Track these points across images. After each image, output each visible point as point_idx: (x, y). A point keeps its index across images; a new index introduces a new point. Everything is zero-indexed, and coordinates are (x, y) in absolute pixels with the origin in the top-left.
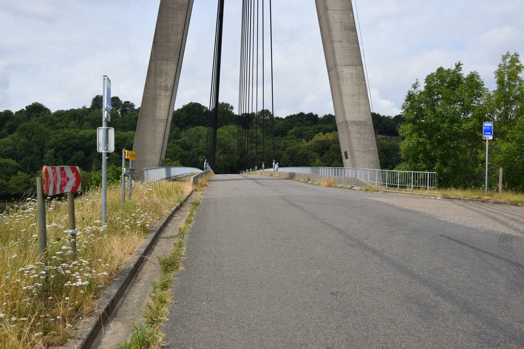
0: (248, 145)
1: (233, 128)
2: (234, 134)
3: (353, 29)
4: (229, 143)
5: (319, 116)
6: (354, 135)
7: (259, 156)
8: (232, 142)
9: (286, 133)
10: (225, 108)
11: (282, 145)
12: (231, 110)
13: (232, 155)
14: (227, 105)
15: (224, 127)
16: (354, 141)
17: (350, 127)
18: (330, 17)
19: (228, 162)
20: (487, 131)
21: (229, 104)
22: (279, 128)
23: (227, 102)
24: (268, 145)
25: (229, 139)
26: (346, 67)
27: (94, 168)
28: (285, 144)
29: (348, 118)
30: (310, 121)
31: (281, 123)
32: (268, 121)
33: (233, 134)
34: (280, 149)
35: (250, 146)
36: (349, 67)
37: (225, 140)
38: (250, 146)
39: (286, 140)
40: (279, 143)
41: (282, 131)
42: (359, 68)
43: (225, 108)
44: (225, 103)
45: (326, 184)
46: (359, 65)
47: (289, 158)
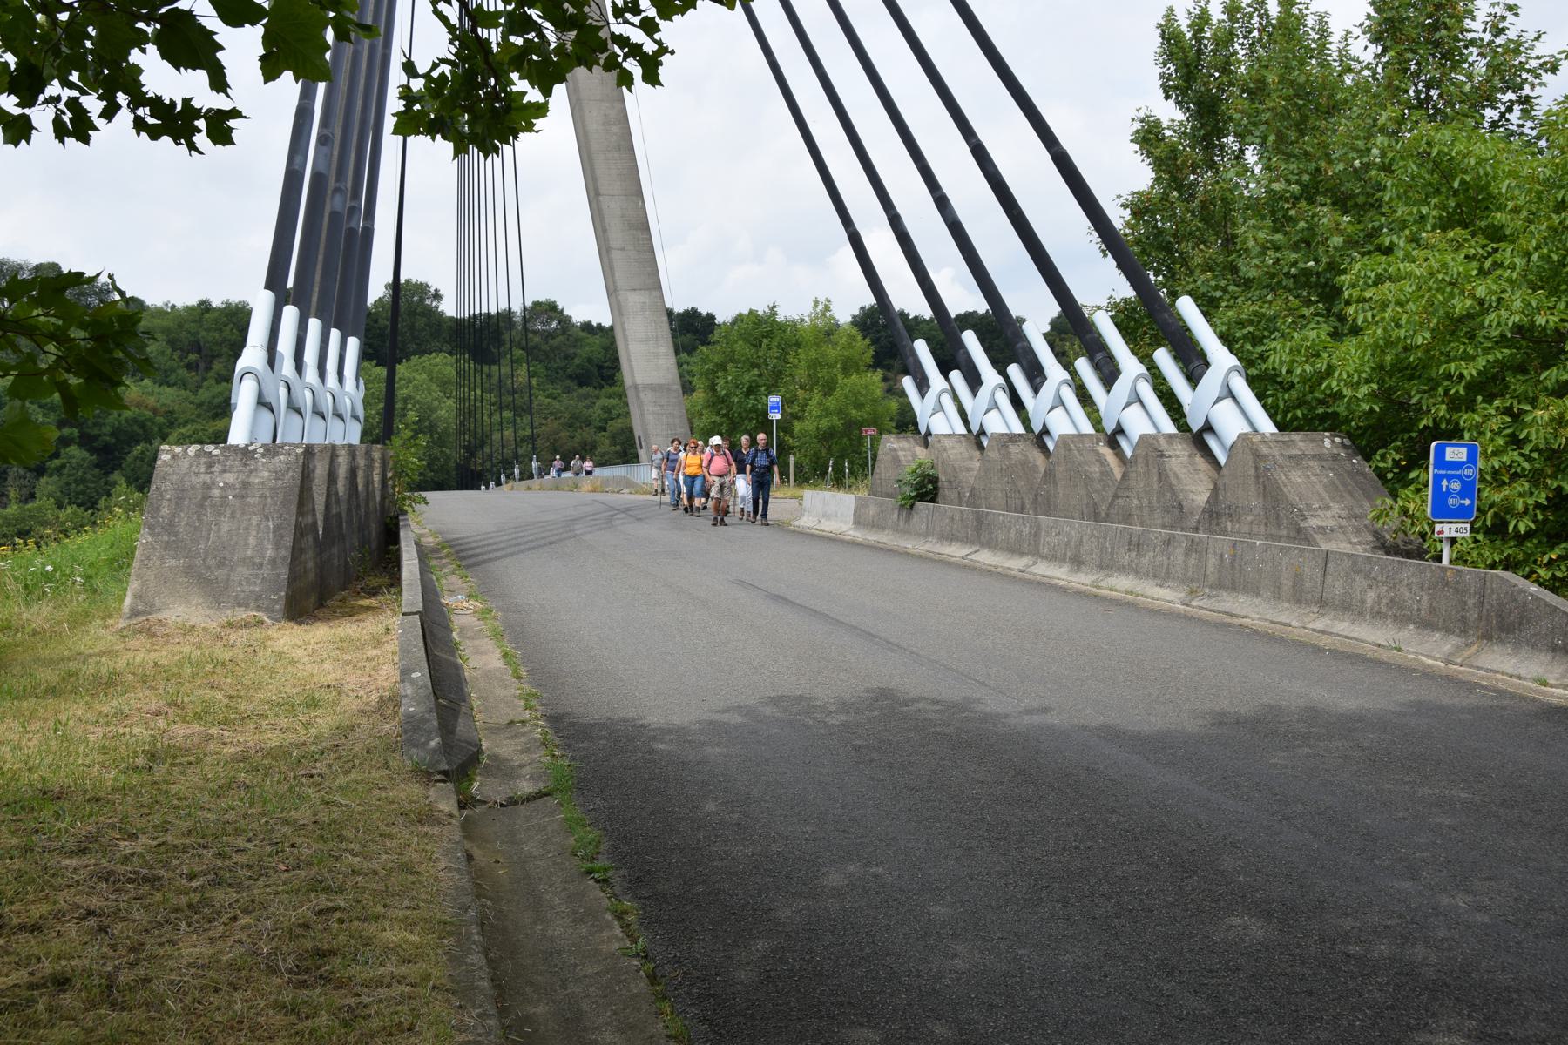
0: (490, 416)
1: (443, 363)
2: (445, 383)
3: (641, 226)
4: (434, 410)
5: (719, 320)
6: (648, 408)
7: (524, 448)
8: (442, 409)
9: (614, 375)
10: (415, 299)
11: (596, 413)
12: (434, 304)
13: (441, 447)
14: (422, 288)
15: (415, 359)
16: (650, 418)
17: (642, 395)
18: (604, 207)
19: (432, 471)
20: (772, 408)
21: (427, 286)
22: (589, 360)
23: (422, 280)
24: (552, 413)
25: (429, 399)
26: (633, 292)
27: (12, 495)
28: (607, 410)
29: (639, 380)
30: (689, 335)
31: (597, 342)
32: (553, 338)
33: (444, 384)
34: (589, 425)
35: (496, 417)
36: (638, 292)
37: (418, 402)
38: (496, 417)
39: (610, 397)
40: (587, 407)
41: (600, 368)
42: (655, 293)
43: (415, 299)
44: (414, 281)
45: (590, 488)
46: (655, 289)
47: (617, 452)
